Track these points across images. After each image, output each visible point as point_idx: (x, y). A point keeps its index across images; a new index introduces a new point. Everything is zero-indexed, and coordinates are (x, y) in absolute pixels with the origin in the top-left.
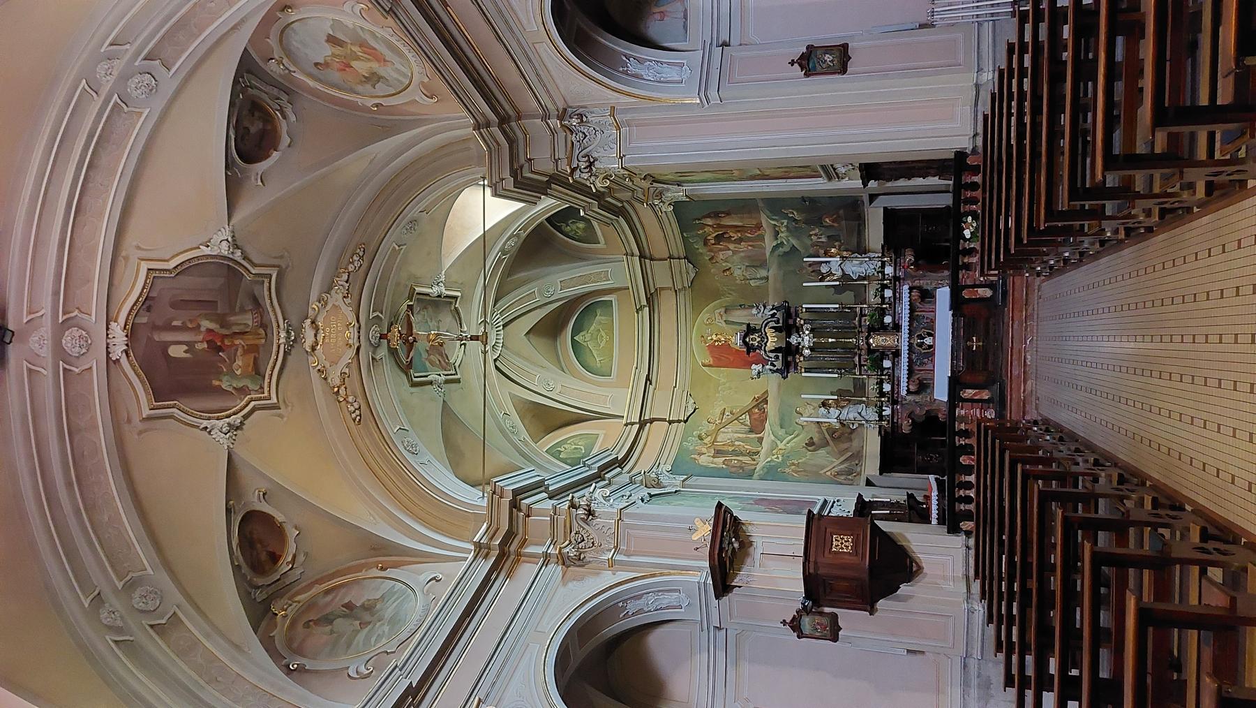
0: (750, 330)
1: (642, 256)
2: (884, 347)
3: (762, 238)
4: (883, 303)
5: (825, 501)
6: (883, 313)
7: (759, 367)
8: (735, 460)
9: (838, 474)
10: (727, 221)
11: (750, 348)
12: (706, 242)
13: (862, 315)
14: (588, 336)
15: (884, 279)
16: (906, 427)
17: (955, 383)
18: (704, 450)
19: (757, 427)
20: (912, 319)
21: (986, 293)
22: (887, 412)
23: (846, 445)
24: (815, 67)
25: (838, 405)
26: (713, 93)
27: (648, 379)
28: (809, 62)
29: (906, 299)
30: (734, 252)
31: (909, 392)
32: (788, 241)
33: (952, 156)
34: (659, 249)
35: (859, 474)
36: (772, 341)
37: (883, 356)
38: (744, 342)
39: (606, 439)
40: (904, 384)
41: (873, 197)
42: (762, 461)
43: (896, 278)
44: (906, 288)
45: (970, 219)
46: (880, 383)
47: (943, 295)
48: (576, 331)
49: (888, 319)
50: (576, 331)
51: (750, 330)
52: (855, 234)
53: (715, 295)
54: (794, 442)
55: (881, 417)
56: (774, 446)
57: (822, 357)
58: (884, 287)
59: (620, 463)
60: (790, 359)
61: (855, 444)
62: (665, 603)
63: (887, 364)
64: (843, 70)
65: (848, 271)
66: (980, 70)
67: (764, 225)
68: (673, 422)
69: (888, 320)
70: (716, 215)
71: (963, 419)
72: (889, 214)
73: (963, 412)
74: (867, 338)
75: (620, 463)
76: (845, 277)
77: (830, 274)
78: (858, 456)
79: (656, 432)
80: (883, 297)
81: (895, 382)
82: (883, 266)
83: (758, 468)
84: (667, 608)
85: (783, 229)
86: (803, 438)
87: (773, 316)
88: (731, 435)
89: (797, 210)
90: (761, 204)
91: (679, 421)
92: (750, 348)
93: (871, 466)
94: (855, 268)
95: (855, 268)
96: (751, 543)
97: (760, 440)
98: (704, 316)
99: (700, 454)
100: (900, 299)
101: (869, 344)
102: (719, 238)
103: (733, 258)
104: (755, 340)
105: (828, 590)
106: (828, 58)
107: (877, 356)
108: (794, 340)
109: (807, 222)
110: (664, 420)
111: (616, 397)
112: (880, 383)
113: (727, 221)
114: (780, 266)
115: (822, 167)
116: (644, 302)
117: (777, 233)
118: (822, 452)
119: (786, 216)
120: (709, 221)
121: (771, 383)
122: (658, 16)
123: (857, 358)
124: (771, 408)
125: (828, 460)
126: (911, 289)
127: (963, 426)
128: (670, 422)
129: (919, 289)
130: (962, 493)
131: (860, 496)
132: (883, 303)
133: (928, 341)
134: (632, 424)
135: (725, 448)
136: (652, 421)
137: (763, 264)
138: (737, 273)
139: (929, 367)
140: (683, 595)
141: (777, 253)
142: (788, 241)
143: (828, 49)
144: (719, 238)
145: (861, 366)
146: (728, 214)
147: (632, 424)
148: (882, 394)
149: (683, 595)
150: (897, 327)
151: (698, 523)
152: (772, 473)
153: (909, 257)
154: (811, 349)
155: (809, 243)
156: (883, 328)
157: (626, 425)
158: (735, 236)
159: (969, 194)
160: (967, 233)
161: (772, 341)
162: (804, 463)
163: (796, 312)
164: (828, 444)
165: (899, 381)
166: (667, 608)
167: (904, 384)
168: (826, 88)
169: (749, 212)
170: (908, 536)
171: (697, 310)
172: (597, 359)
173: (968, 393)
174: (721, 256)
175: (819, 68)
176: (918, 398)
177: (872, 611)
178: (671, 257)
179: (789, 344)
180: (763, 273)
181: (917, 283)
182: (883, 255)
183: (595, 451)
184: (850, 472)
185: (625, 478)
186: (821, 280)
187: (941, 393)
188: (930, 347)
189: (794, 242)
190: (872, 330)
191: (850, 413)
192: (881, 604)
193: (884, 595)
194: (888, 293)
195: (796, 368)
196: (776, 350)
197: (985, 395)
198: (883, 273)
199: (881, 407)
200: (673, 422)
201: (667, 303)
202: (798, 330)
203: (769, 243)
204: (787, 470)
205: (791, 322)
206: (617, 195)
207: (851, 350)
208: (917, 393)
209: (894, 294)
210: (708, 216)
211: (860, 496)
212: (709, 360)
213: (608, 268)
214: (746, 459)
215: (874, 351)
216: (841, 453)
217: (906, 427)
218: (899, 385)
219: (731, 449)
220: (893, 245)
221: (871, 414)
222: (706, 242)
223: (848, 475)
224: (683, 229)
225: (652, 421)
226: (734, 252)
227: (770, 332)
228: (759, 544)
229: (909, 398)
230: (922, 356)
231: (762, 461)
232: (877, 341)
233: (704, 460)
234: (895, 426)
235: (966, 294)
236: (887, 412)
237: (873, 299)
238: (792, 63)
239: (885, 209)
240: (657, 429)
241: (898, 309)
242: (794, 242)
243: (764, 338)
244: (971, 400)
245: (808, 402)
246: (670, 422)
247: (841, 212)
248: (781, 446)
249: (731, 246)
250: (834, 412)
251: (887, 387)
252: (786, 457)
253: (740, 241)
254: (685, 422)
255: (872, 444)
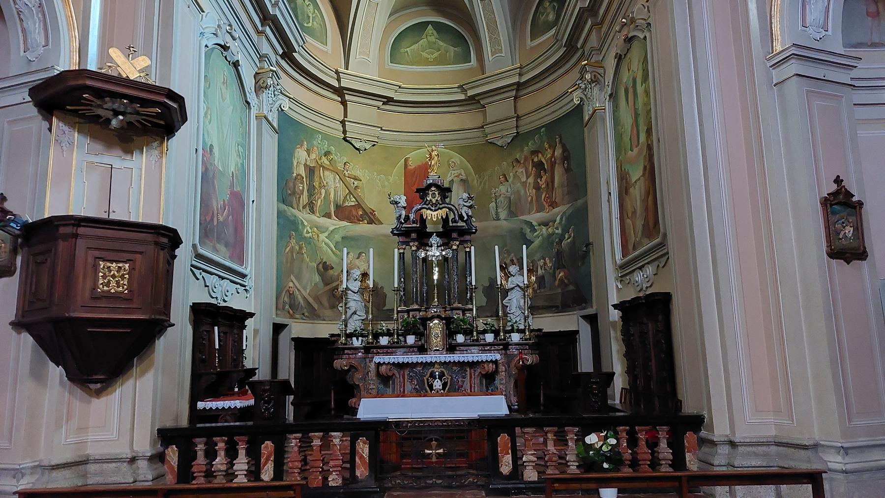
0: (445, 191)
1: (519, 86)
2: (428, 337)
3: (540, 209)
4: (479, 333)
5: (244, 276)
6: (467, 333)
7: (403, 203)
8: (303, 187)
9: (291, 295)
10: (558, 172)
11: (423, 192)
12: (535, 152)
13: (464, 311)
14: (432, 39)
15: (506, 332)
16: (340, 363)
17: (376, 430)
18: (313, 156)
19: (342, 212)
20: (462, 365)
21: (506, 465)
22: (356, 343)
23: (325, 302)
24: (834, 213)
25: (362, 291)
26: (793, 67)
27: (389, 100)
28: (841, 204)
29: (484, 357)
30: (524, 184)
31: (379, 365)
32: (538, 237)
33: (689, 408)
34: (527, 104)
35: (292, 317)
36: (433, 216)
37: (419, 335)
38: (430, 185)
39: (321, 50)
40: (387, 359)
41: (592, 320)
42: (304, 216)
43: (506, 346)
44: (498, 356)
45: (613, 441)
46: (389, 333)
47: (496, 406)
48: (437, 26)
49: (460, 338)
50: (437, 26)
51: (445, 191)
52: (546, 304)
53: (479, 169)
54: (326, 247)
55: (350, 336)
56: (321, 229)
57: (414, 272)
58: (496, 333)
59: (288, 55)
60: (413, 235)
61: (328, 313)
62: (29, 24)
63: (411, 339)
64: (835, 253)
65: (511, 295)
66: (846, 450)
67: (556, 210)
68: (344, 126)
69: (460, 338)
70: (566, 157)
71: (326, 444)
72: (571, 337)
73: (336, 441)
74: (439, 317)
75: (288, 55)
76: (506, 292)
77: (507, 275)
78: (313, 315)
79: (331, 106)
80: (484, 332)
81: (388, 349)
82: (519, 331)
83: (295, 212)
84: (24, 31)
85: (550, 230)
86: (330, 257)
87: (461, 217)
88: (332, 186)
89: (573, 242)
90: (580, 202)
91: (345, 132)
92: (423, 192)
93: (300, 329)
94: (515, 303)
95: (515, 303)
96: (129, 151)
97: (328, 215)
98: (457, 158)
99: (308, 152)
100: (484, 351)
101: (432, 318)
102: (539, 166)
103: (519, 182)
104: (433, 196)
105: (39, 259)
106: (849, 231)
107: (419, 328)
108: (434, 240)
109: (559, 254)
110: (346, 115)
111: (368, 60)
112: (389, 333)
113: (558, 172)
114: (511, 231)
115: (662, 245)
116: (470, 93)
117: (546, 224)
118: (317, 278)
119: (565, 230)
120: (558, 152)
121: (389, 220)
122: (872, 8)
123: (416, 307)
124: (363, 228)
125: (307, 284)
126: (495, 362)
127: (317, 442)
128: (343, 123)
129: (496, 372)
130: (221, 445)
131: (251, 315)
132: (479, 333)
133: (437, 384)
134: (339, 80)
135: (316, 179)
136: (344, 103)
137: (512, 214)
138: (503, 189)
139: (409, 387)
140: (41, 50)
141: (524, 226)
142: (538, 237)
143: (859, 230)
144: (539, 166)
145: (408, 312)
146: (568, 170)
147: (339, 80)
148: (376, 336)
149: (41, 50)
150: (452, 348)
151: (143, 62)
152: (287, 226)
153: (531, 359)
154: (425, 260)
155: (536, 258)
156: (450, 334)
157: (337, 72)
158: (542, 183)
159: (642, 436)
160: (592, 439)
161: (433, 216)
162: (303, 260)
163: (466, 241)
164: (326, 284)
165: (391, 353)
166: (24, 31)
167: (387, 359)
168: (802, 233)
169: (569, 193)
170: (150, 376)
171: (462, 151)
172: (410, 49)
173: (363, 449)
174: (521, 170)
175: (833, 219)
176: (372, 374)
177: (18, 325)
178: (518, 117)
179: (430, 235)
180: (503, 214)
181: (502, 368)
182: (532, 331)
183: (308, 38)
184: (294, 306)
185: (266, 49)
186: (501, 266)
187: (370, 409)
188: (431, 387)
189: (537, 242)
190: (448, 321)
191: (355, 302)
192: (27, 339)
193: (40, 340)
194: (489, 338)
195: (403, 243)
196: (423, 221)
197: (361, 472)
198: (512, 331)
199: (362, 336)
200: (344, 126)
201: (467, 119)
202: (446, 245)
203: (535, 217)
204: (293, 241)
205: (454, 235)
206: (594, 33)
207: (426, 302)
208: (378, 374)
209: (489, 344)
210: (565, 150)
211: (251, 315)
212: (412, 165)
213: (505, 52)
214: (304, 199)
215: (425, 326)
216: (317, 299)
217: (340, 363)
218: (387, 354)
219: (316, 184)
220: (543, 342)
221: (354, 325)
222: (535, 152)
223: (288, 303)
224: (550, 126)
225: (344, 103)
226: (524, 184)
227: (442, 213)
228: (128, 164)
229: (373, 366)
230: (421, 382)
231: (304, 216)
232: (436, 326)
233: (301, 155)
234: (340, 352)
235: (503, 439)
236: (356, 343)
237: (480, 324)
238: (838, 181)
239: (577, 332)
240: (336, 110)
241: (475, 349)
242: (537, 242)
243: (436, 207)
244: (353, 452)
245: (367, 262)
246: (343, 123)
247: (571, 287)
248: (323, 236)
249: (531, 180)
250: (355, 286)
251: (384, 341)
252: (309, 241)
253: (537, 187)
254: (345, 139)
255: (323, 330)
